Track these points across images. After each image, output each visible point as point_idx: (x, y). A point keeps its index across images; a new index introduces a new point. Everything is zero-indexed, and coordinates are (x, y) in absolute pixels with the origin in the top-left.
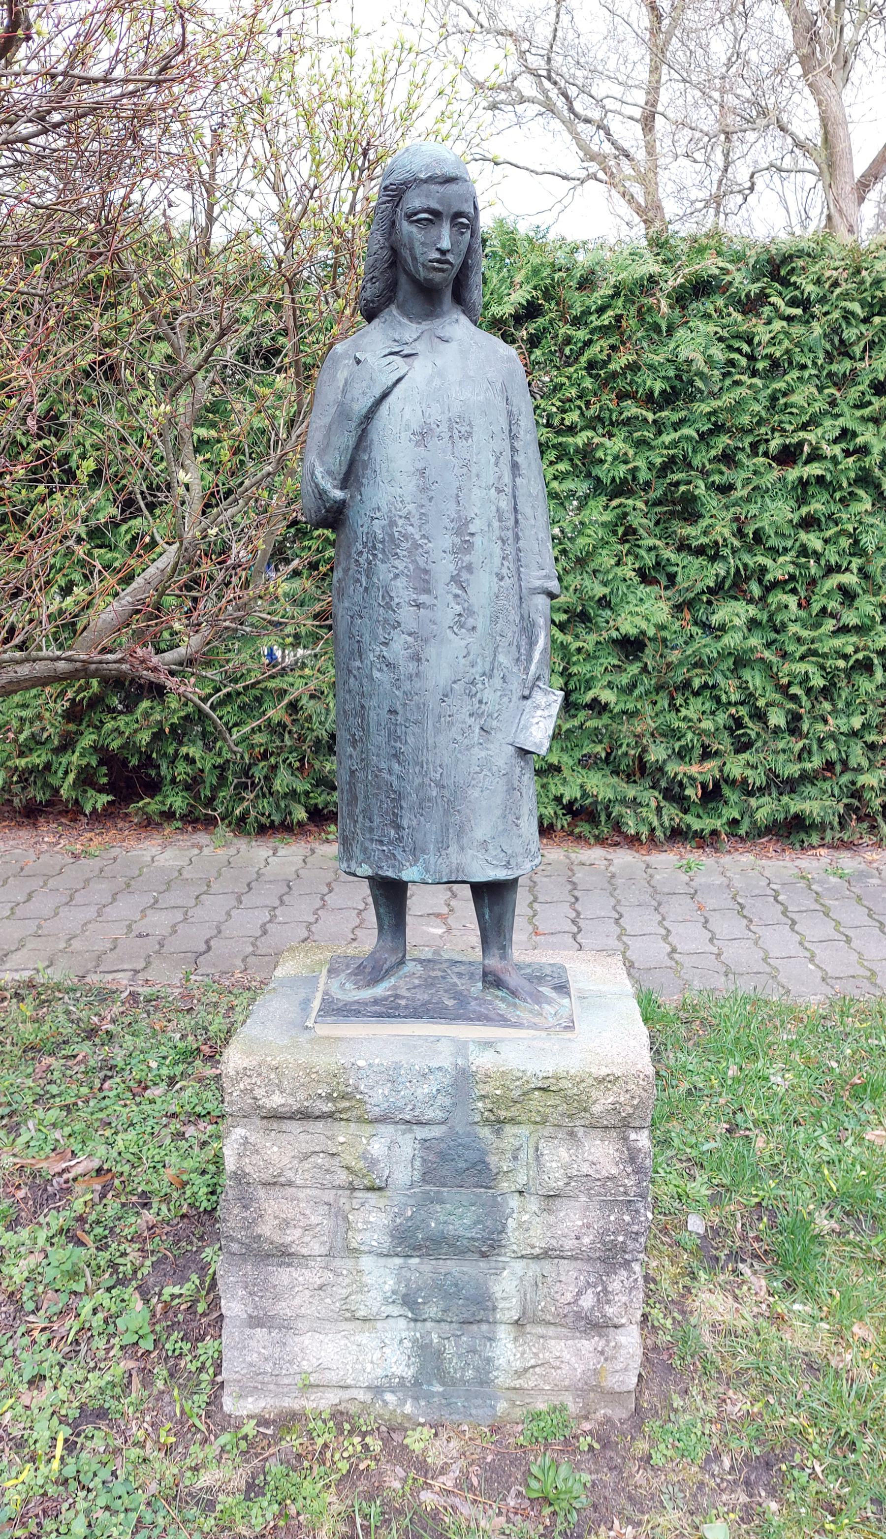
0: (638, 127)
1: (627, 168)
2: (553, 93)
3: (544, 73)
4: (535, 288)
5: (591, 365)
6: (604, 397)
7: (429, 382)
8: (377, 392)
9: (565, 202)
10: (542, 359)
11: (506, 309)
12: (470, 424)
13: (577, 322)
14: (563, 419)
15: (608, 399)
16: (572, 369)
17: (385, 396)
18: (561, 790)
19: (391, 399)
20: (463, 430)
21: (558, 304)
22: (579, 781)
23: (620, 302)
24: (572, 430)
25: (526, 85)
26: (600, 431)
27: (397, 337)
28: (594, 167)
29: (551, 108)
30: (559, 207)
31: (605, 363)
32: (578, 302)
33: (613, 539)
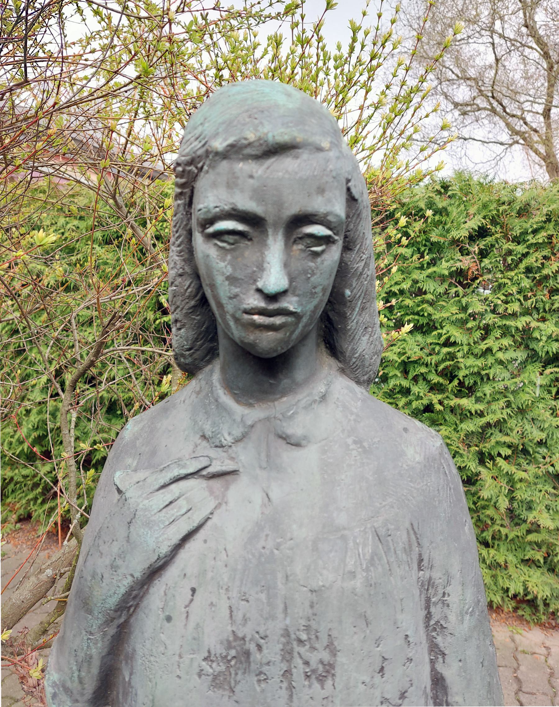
0: (542, 119)
1: (536, 138)
2: (495, 104)
3: (490, 94)
4: (484, 218)
5: (529, 270)
6: (539, 293)
7: (253, 538)
8: (137, 566)
9: (501, 156)
10: (490, 267)
11: (462, 233)
12: (331, 648)
13: (517, 240)
14: (507, 309)
15: (543, 295)
16: (512, 274)
17: (155, 572)
18: (507, 584)
19: (172, 574)
20: (314, 658)
21: (502, 227)
22: (522, 579)
23: (551, 225)
24: (514, 315)
25: (481, 102)
26: (536, 316)
27: (208, 429)
28: (517, 138)
29: (493, 111)
30: (498, 158)
31: (539, 269)
32: (517, 226)
33: (548, 396)
